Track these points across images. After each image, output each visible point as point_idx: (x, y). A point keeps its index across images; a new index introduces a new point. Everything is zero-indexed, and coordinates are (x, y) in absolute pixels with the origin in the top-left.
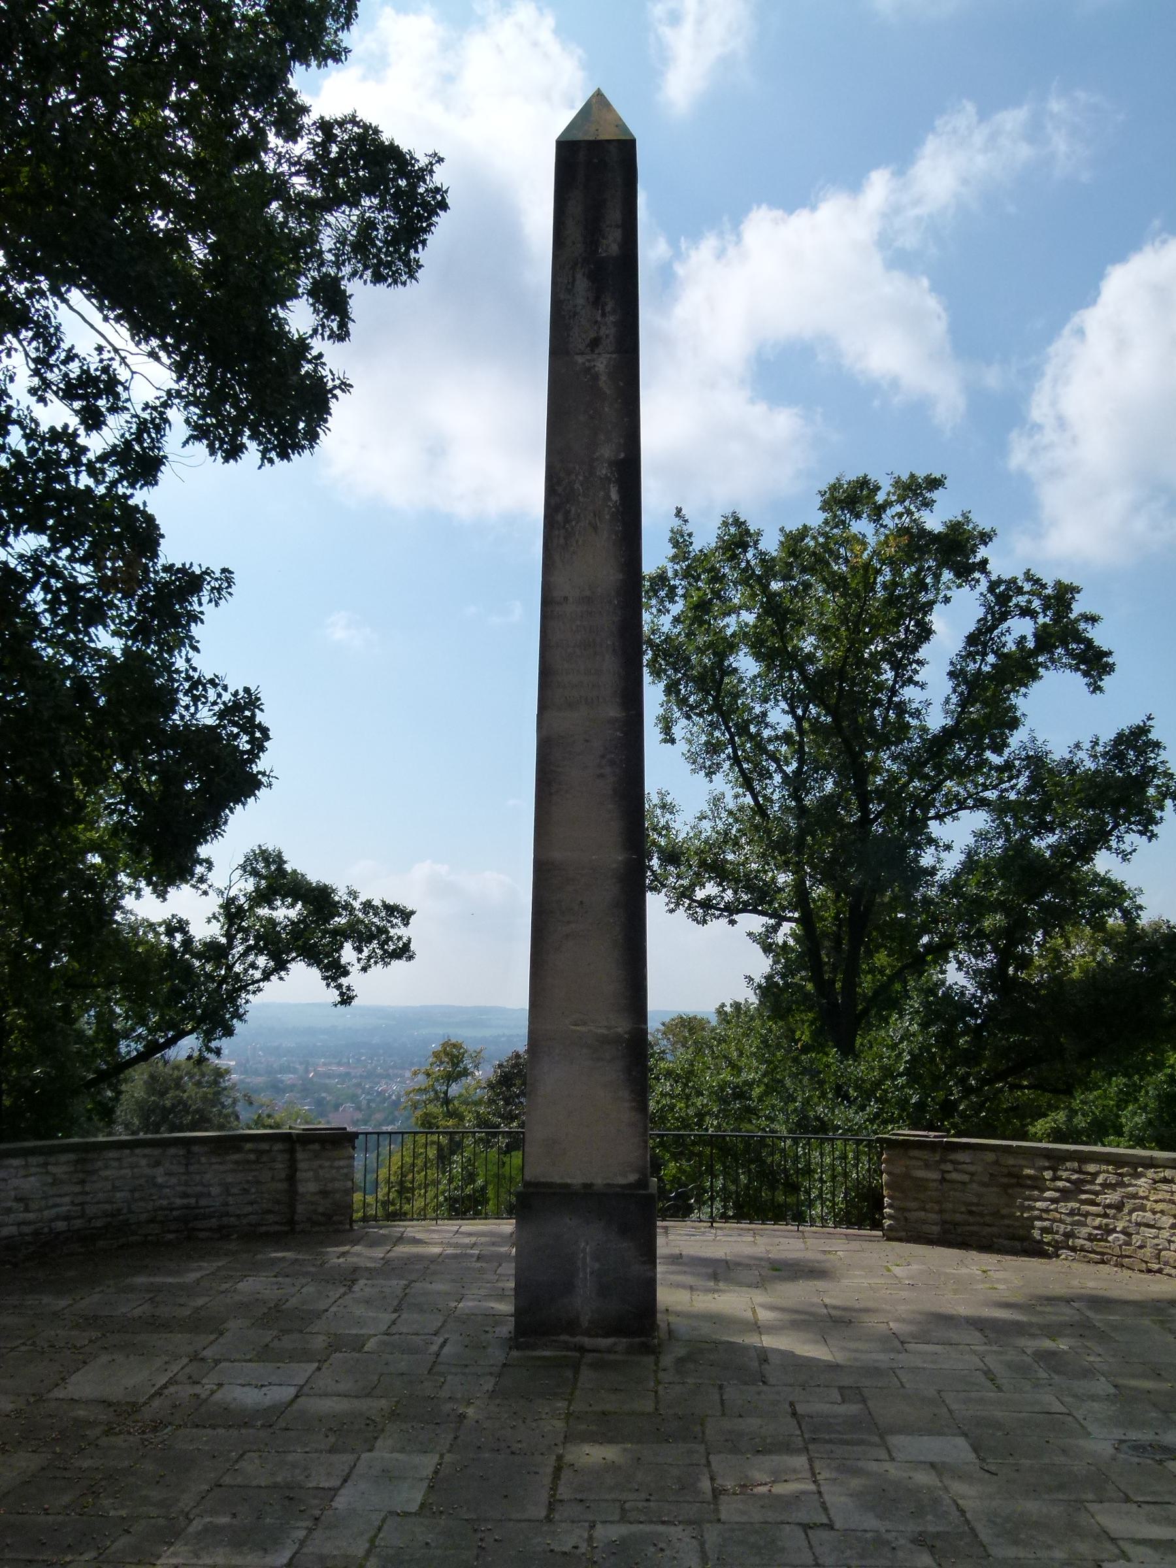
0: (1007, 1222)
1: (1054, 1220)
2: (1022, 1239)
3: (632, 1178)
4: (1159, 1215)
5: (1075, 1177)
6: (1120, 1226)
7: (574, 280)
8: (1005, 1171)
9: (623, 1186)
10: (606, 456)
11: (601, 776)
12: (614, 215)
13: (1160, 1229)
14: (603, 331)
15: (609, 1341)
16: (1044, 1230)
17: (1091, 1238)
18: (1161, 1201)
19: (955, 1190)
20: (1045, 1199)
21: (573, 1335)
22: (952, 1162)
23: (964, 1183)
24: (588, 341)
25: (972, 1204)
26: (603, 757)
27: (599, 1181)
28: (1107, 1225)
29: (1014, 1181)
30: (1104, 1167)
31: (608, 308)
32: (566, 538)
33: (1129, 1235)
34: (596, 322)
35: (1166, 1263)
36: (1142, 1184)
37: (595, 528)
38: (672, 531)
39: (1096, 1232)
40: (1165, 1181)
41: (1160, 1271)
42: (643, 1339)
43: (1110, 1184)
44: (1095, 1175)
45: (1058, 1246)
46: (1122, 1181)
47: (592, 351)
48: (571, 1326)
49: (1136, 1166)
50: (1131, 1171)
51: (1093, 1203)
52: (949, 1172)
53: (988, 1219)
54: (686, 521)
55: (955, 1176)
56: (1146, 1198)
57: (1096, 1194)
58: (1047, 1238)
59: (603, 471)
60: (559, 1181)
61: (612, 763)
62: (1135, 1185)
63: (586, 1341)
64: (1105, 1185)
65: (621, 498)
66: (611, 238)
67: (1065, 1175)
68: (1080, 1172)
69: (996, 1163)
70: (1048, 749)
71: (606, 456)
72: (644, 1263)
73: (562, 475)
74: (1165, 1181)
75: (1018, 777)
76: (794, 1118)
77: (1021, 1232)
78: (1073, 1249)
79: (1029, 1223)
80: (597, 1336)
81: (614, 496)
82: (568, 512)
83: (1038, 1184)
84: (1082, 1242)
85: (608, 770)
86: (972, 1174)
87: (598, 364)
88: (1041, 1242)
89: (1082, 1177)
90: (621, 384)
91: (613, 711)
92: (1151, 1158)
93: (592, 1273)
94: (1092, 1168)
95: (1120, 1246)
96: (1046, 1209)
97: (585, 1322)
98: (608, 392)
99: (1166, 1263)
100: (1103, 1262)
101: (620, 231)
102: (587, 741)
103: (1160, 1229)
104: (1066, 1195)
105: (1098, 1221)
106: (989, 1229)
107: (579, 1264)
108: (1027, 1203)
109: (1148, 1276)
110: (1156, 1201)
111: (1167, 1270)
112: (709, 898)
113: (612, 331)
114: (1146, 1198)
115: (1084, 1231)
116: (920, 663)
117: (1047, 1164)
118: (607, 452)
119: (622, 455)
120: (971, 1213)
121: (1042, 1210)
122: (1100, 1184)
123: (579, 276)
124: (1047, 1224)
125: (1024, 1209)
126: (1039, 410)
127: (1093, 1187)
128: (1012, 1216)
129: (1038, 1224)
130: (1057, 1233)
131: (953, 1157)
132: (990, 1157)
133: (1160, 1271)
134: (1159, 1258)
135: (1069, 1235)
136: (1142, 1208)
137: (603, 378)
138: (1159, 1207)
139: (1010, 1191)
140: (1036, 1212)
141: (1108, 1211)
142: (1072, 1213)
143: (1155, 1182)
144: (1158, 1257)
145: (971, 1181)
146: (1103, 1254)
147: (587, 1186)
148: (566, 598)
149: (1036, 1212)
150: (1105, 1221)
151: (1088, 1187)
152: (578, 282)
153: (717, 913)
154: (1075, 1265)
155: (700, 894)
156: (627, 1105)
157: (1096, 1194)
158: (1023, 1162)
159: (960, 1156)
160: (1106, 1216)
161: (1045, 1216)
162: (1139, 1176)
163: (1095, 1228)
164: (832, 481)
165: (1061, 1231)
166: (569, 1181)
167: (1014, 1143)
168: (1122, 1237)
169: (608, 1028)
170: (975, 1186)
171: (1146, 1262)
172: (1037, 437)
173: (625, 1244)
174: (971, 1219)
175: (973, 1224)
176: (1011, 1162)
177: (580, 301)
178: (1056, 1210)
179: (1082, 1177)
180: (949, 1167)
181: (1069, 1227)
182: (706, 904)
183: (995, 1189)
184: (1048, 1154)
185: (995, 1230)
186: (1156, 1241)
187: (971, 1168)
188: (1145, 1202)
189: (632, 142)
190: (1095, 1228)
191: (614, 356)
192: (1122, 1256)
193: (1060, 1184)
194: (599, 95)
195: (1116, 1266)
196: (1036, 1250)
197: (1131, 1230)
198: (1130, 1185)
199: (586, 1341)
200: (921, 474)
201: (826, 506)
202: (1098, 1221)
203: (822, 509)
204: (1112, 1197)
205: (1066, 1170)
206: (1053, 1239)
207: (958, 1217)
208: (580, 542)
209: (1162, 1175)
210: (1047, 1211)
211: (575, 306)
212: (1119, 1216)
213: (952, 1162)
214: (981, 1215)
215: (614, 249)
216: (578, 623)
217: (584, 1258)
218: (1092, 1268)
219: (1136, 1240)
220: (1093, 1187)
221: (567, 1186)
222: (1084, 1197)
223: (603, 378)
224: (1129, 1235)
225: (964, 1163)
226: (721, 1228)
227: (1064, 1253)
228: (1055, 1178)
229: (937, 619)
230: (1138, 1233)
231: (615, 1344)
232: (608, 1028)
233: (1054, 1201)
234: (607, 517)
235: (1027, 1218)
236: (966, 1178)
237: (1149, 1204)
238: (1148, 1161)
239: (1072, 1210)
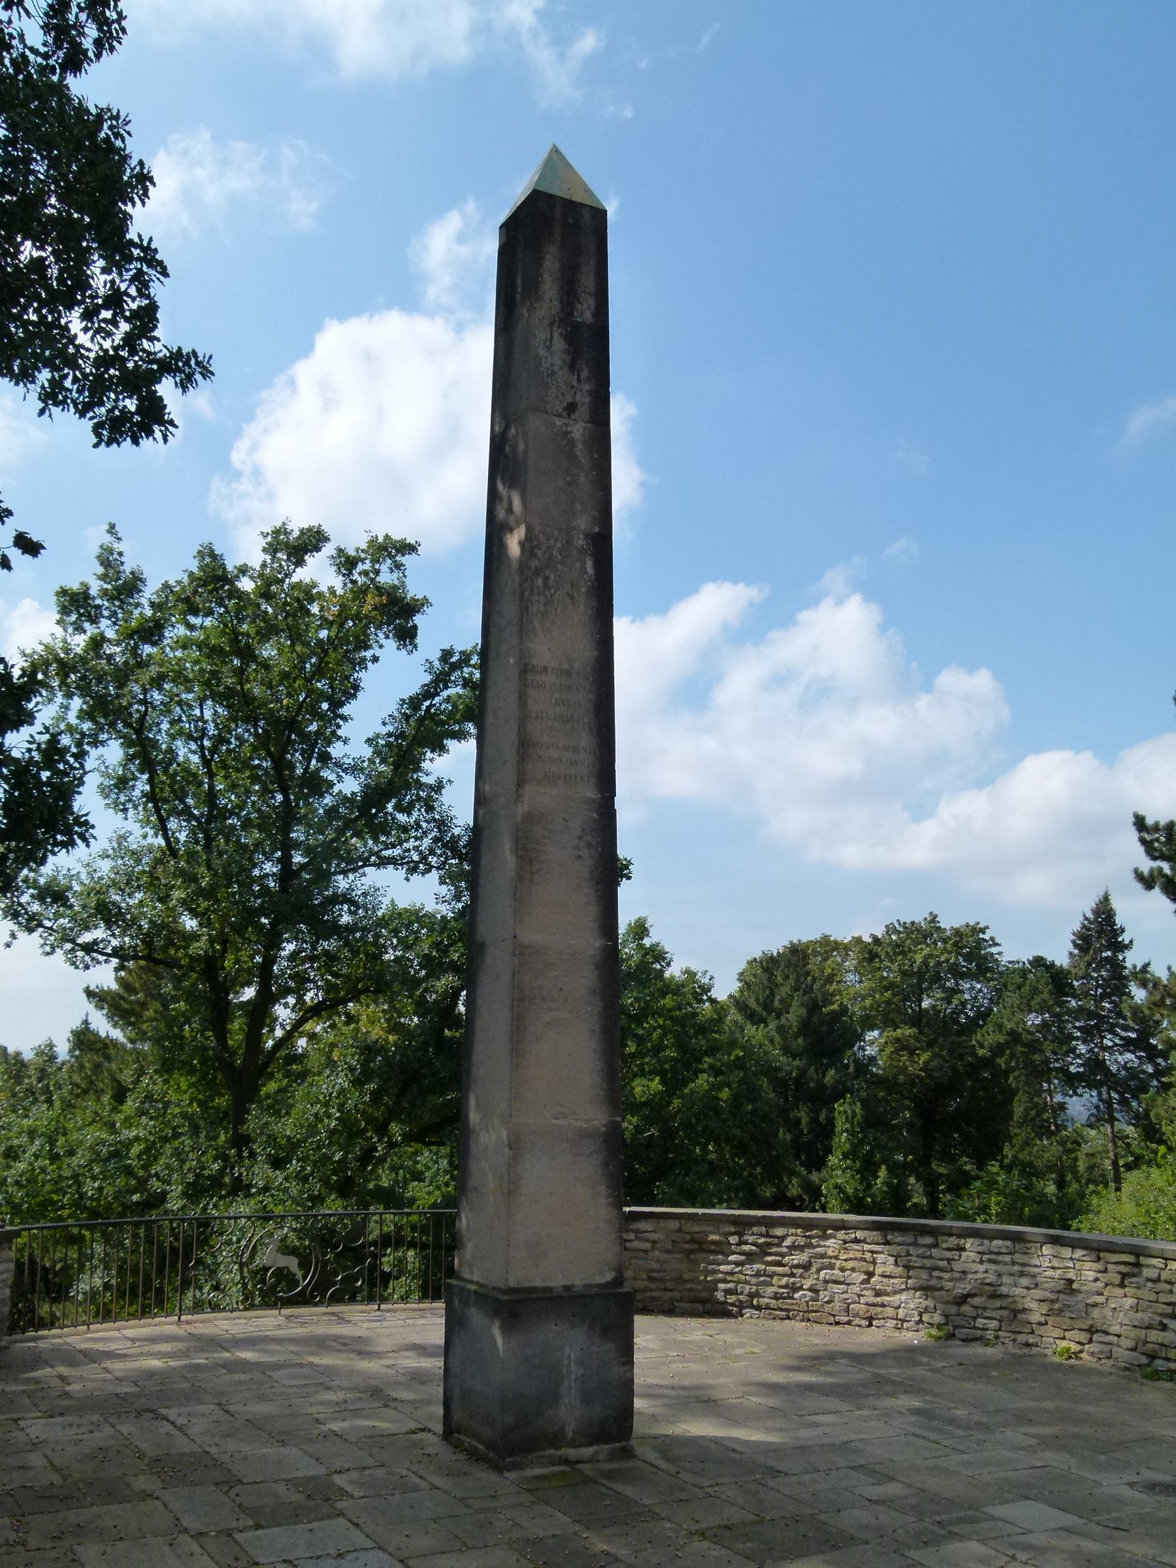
0: (689, 1286)
1: (738, 1282)
2: (704, 1302)
3: (609, 1276)
4: (848, 1273)
5: (762, 1240)
6: (807, 1284)
7: (552, 339)
8: (688, 1237)
9: (601, 1286)
11: (580, 857)
12: (588, 282)
16: (728, 1292)
17: (776, 1297)
18: (851, 1259)
20: (730, 1263)
21: (557, 1448)
22: (633, 1231)
23: (645, 1251)
24: (565, 404)
25: (654, 1271)
26: (580, 838)
28: (794, 1284)
29: (697, 1246)
31: (584, 374)
32: (545, 605)
33: (816, 1291)
34: (572, 387)
35: (856, 1315)
36: (831, 1245)
37: (572, 599)
38: (101, 547)
39: (782, 1290)
40: (856, 1241)
43: (799, 1246)
45: (741, 1306)
48: (556, 1440)
49: (824, 1229)
50: (820, 1233)
51: (779, 1264)
52: (631, 1241)
53: (669, 1285)
54: (119, 539)
55: (636, 1244)
56: (836, 1258)
57: (783, 1255)
58: (731, 1299)
59: (580, 542)
63: (571, 1453)
64: (793, 1247)
65: (596, 573)
66: (585, 306)
67: (751, 1239)
68: (767, 1235)
69: (680, 1230)
70: (452, 813)
72: (624, 1364)
73: (542, 538)
74: (856, 1241)
76: (191, 1178)
77: (705, 1294)
78: (758, 1308)
80: (580, 1446)
81: (590, 570)
82: (546, 578)
83: (722, 1249)
84: (766, 1300)
85: (585, 852)
86: (654, 1242)
88: (725, 1303)
89: (769, 1240)
93: (576, 1380)
94: (779, 1232)
95: (807, 1302)
96: (730, 1272)
99: (856, 1315)
100: (788, 1318)
104: (750, 1257)
105: (784, 1281)
106: (670, 1294)
107: (564, 1371)
108: (710, 1267)
109: (837, 1328)
110: (846, 1260)
111: (857, 1321)
112: (95, 942)
113: (587, 400)
114: (836, 1258)
115: (770, 1290)
117: (733, 1230)
118: (584, 522)
119: (597, 529)
120: (651, 1279)
121: (727, 1273)
122: (788, 1247)
123: (556, 335)
125: (708, 1272)
126: (239, 456)
128: (694, 1280)
129: (721, 1286)
130: (742, 1293)
131: (635, 1226)
132: (674, 1225)
133: (849, 1323)
135: (752, 1295)
136: (831, 1267)
137: (579, 446)
138: (850, 1265)
139: (693, 1257)
141: (795, 1271)
142: (758, 1274)
143: (845, 1242)
144: (847, 1310)
145: (653, 1249)
147: (567, 1288)
148: (545, 668)
150: (792, 1280)
151: (774, 1250)
152: (555, 341)
153: (101, 958)
154: (761, 1322)
155: (87, 938)
156: (604, 1201)
157: (783, 1255)
160: (792, 1275)
161: (729, 1278)
162: (825, 1237)
163: (781, 1287)
164: (279, 525)
165: (747, 1291)
166: (551, 1284)
167: (700, 1211)
170: (657, 1253)
171: (834, 1316)
172: (234, 485)
174: (653, 1286)
175: (655, 1290)
176: (696, 1228)
178: (741, 1272)
179: (769, 1240)
180: (632, 1236)
182: (89, 948)
183: (678, 1256)
185: (677, 1294)
186: (845, 1296)
188: (833, 1261)
190: (781, 1287)
192: (809, 1311)
193: (747, 1248)
194: (555, 150)
195: (802, 1321)
196: (721, 1311)
197: (818, 1287)
199: (571, 1453)
200: (396, 536)
201: (272, 549)
202: (784, 1281)
203: (264, 550)
204: (799, 1258)
205: (753, 1234)
207: (639, 1284)
210: (732, 1273)
212: (806, 1274)
213: (633, 1231)
214: (663, 1280)
215: (588, 317)
216: (557, 695)
217: (569, 1365)
218: (777, 1324)
219: (824, 1296)
221: (550, 1289)
222: (769, 1259)
223: (579, 446)
224: (816, 1291)
226: (388, 1311)
227: (748, 1312)
228: (740, 1243)
231: (597, 1452)
233: (737, 1264)
236: (648, 1246)
237: (838, 1263)
238: (839, 1224)
239: (758, 1271)
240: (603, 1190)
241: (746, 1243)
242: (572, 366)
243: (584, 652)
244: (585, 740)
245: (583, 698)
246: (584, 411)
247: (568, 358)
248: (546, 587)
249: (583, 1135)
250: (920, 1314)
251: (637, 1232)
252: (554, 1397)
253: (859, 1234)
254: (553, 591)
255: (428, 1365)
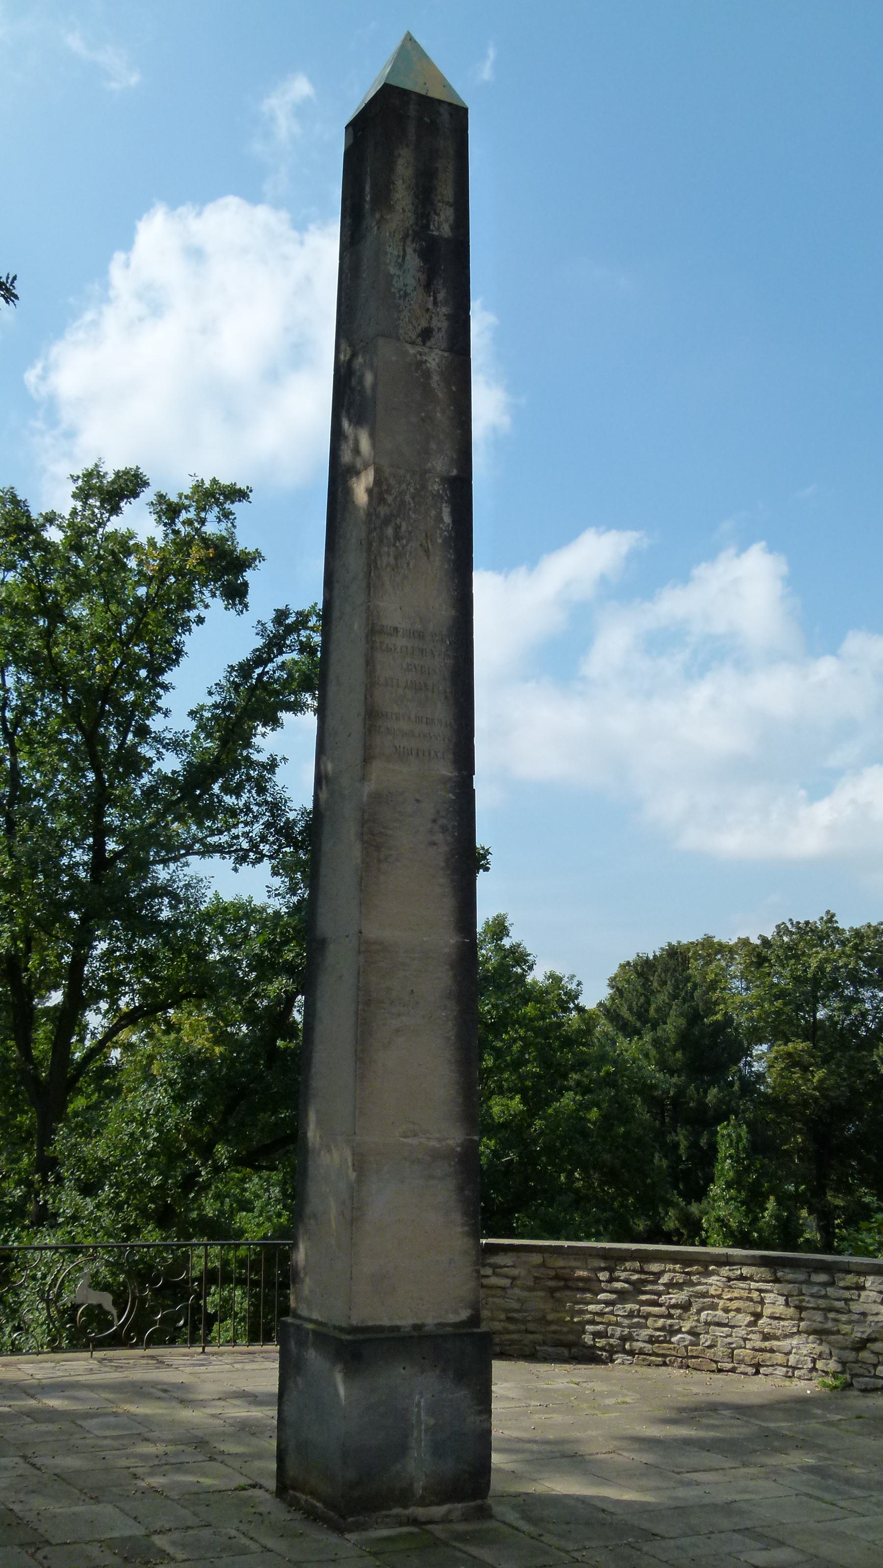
0: (554, 1328)
1: (609, 1324)
2: (569, 1345)
3: (464, 1314)
4: (732, 1314)
5: (636, 1277)
6: (686, 1326)
8: (552, 1273)
9: (456, 1325)
10: (439, 469)
12: (446, 191)
13: (733, 1327)
14: (435, 324)
15: (443, 1509)
16: (597, 1335)
17: (651, 1340)
18: (736, 1298)
19: (494, 1296)
21: (405, 1507)
22: (490, 1265)
23: (503, 1288)
26: (434, 821)
27: (430, 1321)
28: (671, 1326)
29: (562, 1283)
30: (671, 1267)
31: (441, 296)
32: (396, 558)
34: (428, 310)
36: (714, 1283)
37: (427, 551)
39: (658, 1333)
40: (742, 1278)
41: (733, 1370)
42: (479, 1502)
44: (659, 1275)
45: (611, 1351)
46: (691, 1280)
47: (424, 343)
48: (404, 1497)
49: (707, 1264)
53: (531, 1326)
55: (494, 1281)
56: (719, 1297)
57: (659, 1294)
58: (601, 1342)
59: (435, 487)
60: (386, 1322)
61: (444, 830)
62: (706, 1284)
64: (670, 1285)
65: (454, 521)
66: (443, 217)
67: (623, 1275)
68: (642, 1271)
69: (543, 1265)
70: (287, 795)
71: (439, 469)
73: (392, 481)
74: (742, 1278)
75: (252, 823)
77: (571, 1337)
78: (631, 1353)
79: (580, 1328)
81: (447, 518)
82: (398, 528)
83: (590, 1286)
85: (439, 837)
86: (514, 1279)
87: (430, 359)
88: (594, 1347)
89: (643, 1277)
90: (454, 389)
91: (445, 769)
92: (727, 1255)
94: (655, 1267)
95: (686, 1347)
97: (419, 1488)
98: (440, 395)
99: (741, 1362)
100: (665, 1364)
101: (452, 209)
102: (418, 801)
103: (733, 1327)
105: (660, 1322)
106: (531, 1337)
108: (577, 1307)
110: (731, 1300)
111: (742, 1368)
113: (445, 325)
114: (719, 1297)
115: (645, 1333)
116: (165, 687)
117: (603, 1265)
118: (441, 464)
119: (454, 472)
120: (510, 1319)
122: (664, 1284)
124: (600, 1328)
125: (574, 1313)
127: (655, 1287)
129: (590, 1328)
130: (612, 1336)
132: (536, 1259)
133: (733, 1370)
134: (732, 1358)
135: (624, 1339)
136: (713, 1307)
137: (436, 378)
138: (735, 1305)
139: (558, 1295)
140: (588, 1316)
141: (672, 1311)
142: (631, 1315)
143: (729, 1279)
144: (731, 1356)
145: (512, 1286)
146: (664, 1356)
147: (417, 1327)
148: (396, 629)
149: (588, 1316)
150: (669, 1322)
151: (649, 1287)
152: (408, 257)
157: (659, 1294)
158: (573, 1264)
159: (500, 1259)
160: (670, 1316)
162: (709, 1274)
166: (398, 1323)
168: (689, 1337)
169: (440, 1140)
171: (716, 1362)
173: (463, 1393)
175: (513, 1332)
176: (560, 1263)
177: (411, 282)
178: (611, 1313)
179: (643, 1277)
180: (489, 1271)
181: (627, 1331)
184: (605, 1255)
185: (539, 1337)
186: (729, 1340)
187: (515, 1272)
188: (716, 1300)
189: (465, 110)
191: (446, 354)
193: (618, 1285)
194: (409, 38)
195: (681, 1367)
197: (698, 1330)
198: (699, 1284)
200: (225, 481)
202: (660, 1322)
203: (75, 496)
205: (625, 1270)
206: (609, 1344)
208: (411, 566)
209: (739, 1272)
210: (601, 1314)
211: (406, 285)
212: (686, 1315)
213: (490, 1265)
214: (524, 1321)
215: (446, 231)
217: (419, 1413)
218: (652, 1372)
219: (705, 1339)
220: (655, 1287)
221: (397, 1328)
222: (644, 1297)
223: (436, 378)
225: (505, 1266)
226: (213, 1354)
227: (619, 1358)
228: (611, 1280)
229: (192, 641)
230: (707, 1333)
231: (450, 1512)
232: (440, 1140)
233: (607, 1303)
234: (440, 541)
235: (579, 1323)
236: (506, 1282)
237: (721, 1303)
238: (724, 1259)
240: (457, 1217)
241: (617, 1280)
242: (428, 286)
243: (442, 612)
244: (441, 712)
245: (440, 663)
246: (440, 338)
247: (423, 277)
248: (397, 537)
249: (436, 1155)
250: (814, 1361)
251: (495, 1267)
252: (402, 1450)
253: (746, 1271)
254: (404, 542)
255: (259, 1414)
